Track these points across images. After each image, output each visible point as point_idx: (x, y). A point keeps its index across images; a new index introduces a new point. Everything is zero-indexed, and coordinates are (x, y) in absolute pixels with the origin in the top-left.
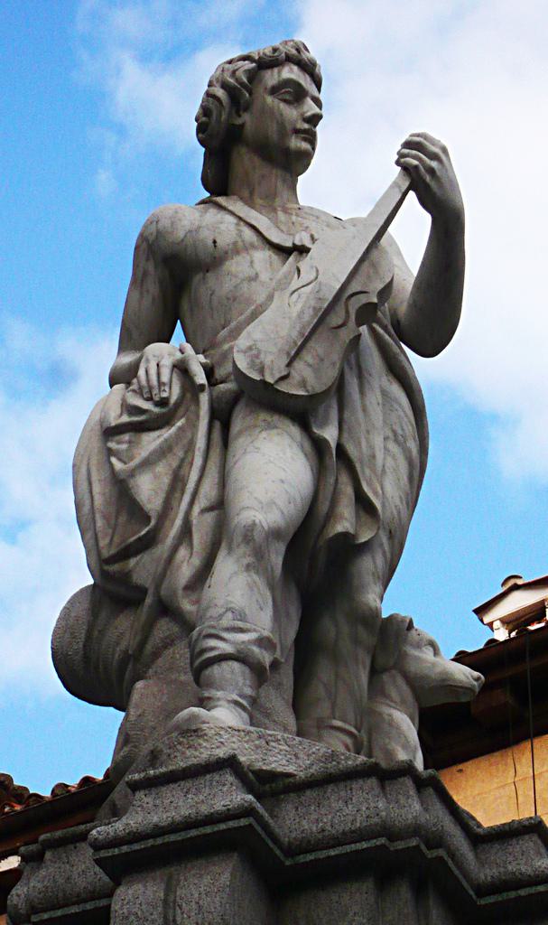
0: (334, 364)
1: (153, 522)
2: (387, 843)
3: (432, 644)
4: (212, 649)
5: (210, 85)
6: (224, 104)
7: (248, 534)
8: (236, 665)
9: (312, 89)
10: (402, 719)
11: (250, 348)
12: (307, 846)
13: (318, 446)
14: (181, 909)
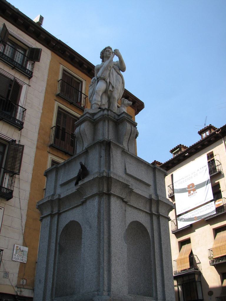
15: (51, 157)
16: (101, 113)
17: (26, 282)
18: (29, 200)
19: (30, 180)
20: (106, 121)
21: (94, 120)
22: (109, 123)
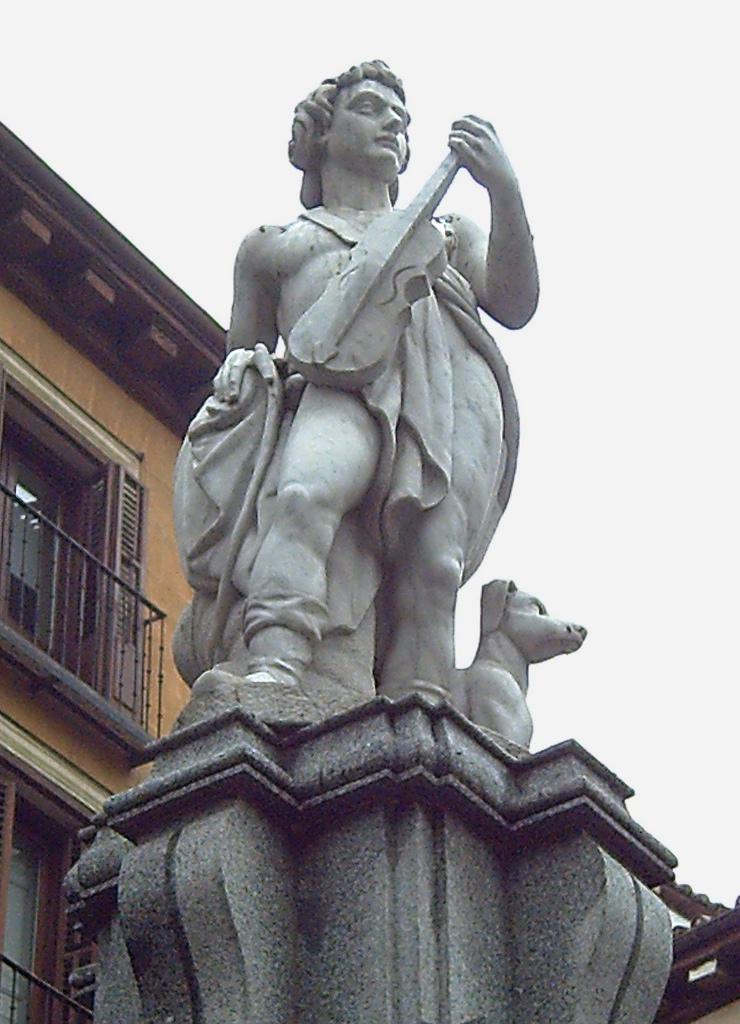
0: (445, 355)
1: (222, 514)
2: (391, 775)
3: (536, 602)
4: (255, 618)
5: (296, 111)
6: (307, 127)
7: (293, 505)
8: (279, 631)
9: (398, 103)
10: (501, 676)
11: (303, 336)
12: (323, 786)
13: (377, 419)
14: (180, 861)
16: (377, 737)
20: (420, 824)
21: (301, 794)
22: (437, 842)
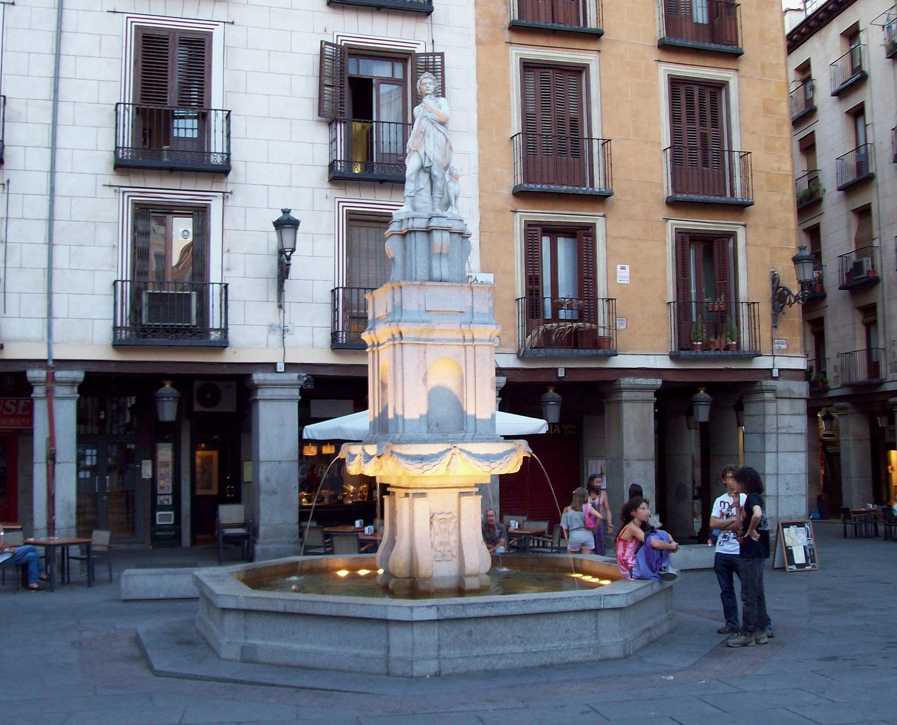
15: (516, 54)
17: (500, 341)
18: (479, 174)
19: (474, 127)
